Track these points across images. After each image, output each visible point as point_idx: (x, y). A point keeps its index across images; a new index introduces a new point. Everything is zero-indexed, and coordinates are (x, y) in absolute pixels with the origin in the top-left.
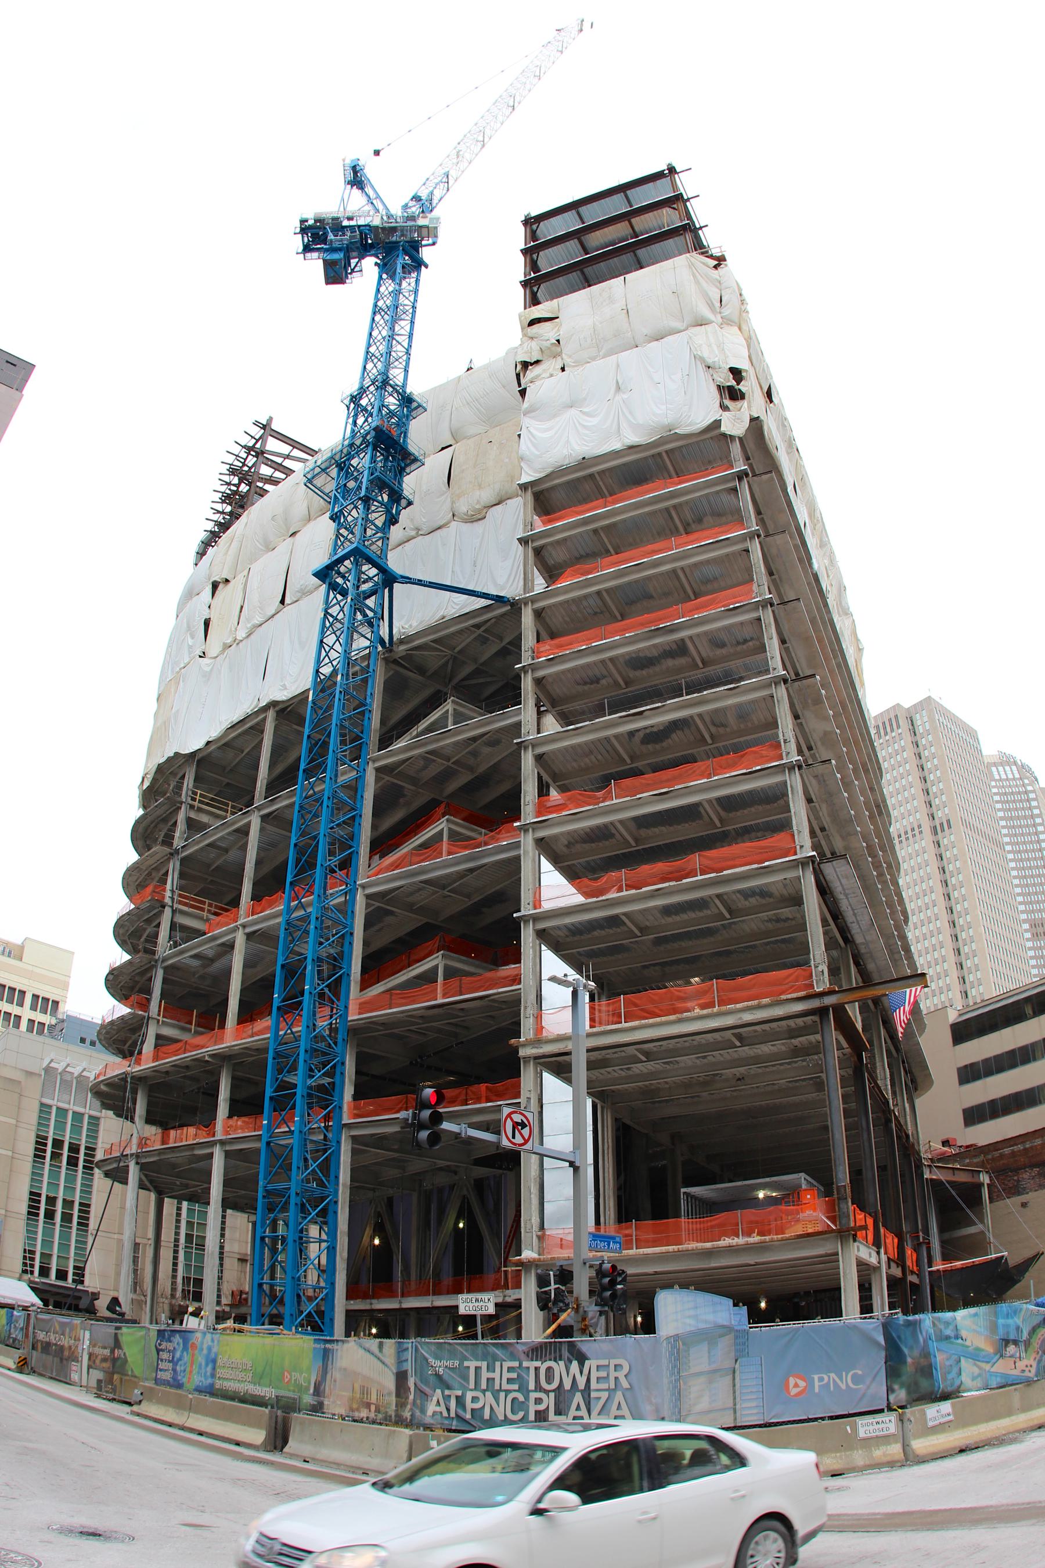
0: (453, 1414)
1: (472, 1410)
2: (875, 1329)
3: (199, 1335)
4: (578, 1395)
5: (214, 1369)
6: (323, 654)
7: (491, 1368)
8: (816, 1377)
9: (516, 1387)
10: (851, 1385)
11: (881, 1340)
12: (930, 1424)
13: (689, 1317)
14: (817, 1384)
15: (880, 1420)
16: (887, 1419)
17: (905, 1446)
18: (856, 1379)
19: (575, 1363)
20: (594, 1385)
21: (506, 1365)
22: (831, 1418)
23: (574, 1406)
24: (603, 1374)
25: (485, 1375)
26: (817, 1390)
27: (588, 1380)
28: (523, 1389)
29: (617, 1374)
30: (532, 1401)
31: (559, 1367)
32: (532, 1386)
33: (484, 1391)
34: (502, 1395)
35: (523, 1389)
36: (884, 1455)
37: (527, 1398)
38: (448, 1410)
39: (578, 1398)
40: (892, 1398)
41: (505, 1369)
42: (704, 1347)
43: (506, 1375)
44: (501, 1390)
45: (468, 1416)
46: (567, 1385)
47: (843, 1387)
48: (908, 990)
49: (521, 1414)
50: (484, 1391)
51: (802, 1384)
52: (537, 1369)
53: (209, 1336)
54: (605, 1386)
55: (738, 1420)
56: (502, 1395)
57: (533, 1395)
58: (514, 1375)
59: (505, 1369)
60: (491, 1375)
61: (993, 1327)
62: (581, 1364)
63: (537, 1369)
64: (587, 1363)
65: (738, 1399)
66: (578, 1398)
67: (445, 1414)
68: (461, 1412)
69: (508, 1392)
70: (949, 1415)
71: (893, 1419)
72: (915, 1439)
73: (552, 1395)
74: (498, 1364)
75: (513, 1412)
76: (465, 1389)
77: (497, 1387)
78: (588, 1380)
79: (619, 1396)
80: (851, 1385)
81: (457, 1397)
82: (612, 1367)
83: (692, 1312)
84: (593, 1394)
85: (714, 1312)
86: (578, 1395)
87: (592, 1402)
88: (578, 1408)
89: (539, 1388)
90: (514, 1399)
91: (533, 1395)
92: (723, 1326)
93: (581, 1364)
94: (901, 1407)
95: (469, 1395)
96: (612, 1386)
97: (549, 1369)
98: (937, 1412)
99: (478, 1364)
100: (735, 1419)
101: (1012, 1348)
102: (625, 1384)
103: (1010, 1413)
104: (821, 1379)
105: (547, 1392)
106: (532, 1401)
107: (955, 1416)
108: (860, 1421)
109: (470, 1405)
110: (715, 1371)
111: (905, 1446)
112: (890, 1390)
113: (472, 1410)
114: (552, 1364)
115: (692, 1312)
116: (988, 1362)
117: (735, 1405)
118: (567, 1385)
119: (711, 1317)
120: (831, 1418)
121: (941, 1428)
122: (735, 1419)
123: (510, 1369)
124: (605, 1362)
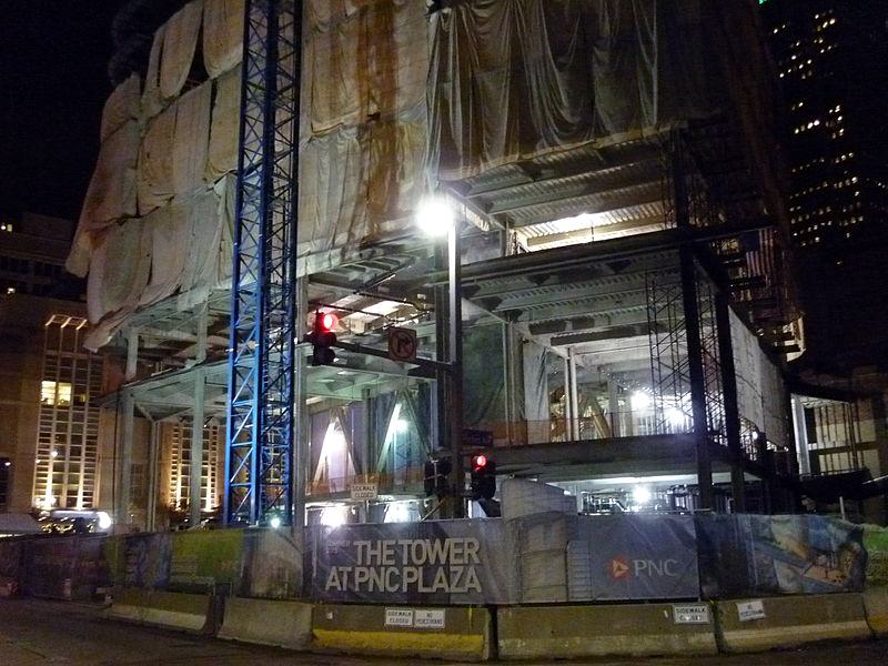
0: (345, 589)
1: (360, 583)
2: (688, 523)
3: (157, 537)
4: (441, 569)
5: (169, 566)
6: (251, 31)
7: (374, 547)
8: (636, 562)
9: (393, 562)
10: (667, 573)
11: (693, 533)
12: (742, 618)
13: (528, 502)
14: (637, 569)
15: (694, 608)
16: (701, 608)
17: (718, 637)
18: (672, 568)
19: (438, 541)
20: (452, 561)
21: (385, 543)
22: (651, 601)
23: (437, 581)
24: (460, 551)
25: (370, 552)
26: (637, 574)
27: (448, 557)
28: (399, 565)
29: (470, 551)
30: (405, 574)
31: (426, 544)
32: (405, 562)
33: (369, 567)
34: (383, 569)
35: (399, 565)
36: (699, 642)
37: (401, 572)
38: (341, 583)
39: (441, 573)
40: (704, 589)
41: (385, 547)
42: (540, 529)
43: (386, 552)
44: (381, 565)
45: (357, 589)
46: (432, 561)
47: (660, 572)
48: (760, 230)
49: (397, 586)
50: (369, 567)
51: (625, 568)
52: (409, 546)
53: (165, 537)
54: (461, 562)
55: (571, 595)
56: (383, 569)
57: (406, 570)
58: (392, 552)
59: (385, 547)
60: (374, 552)
61: (805, 536)
62: (443, 543)
63: (409, 546)
64: (447, 540)
65: (569, 578)
66: (441, 573)
67: (339, 589)
68: (351, 587)
69: (387, 567)
70: (760, 612)
71: (706, 608)
72: (729, 630)
73: (421, 569)
74: (379, 542)
75: (391, 585)
76: (354, 565)
77: (379, 563)
78: (448, 557)
79: (472, 569)
80: (667, 573)
81: (349, 573)
82: (466, 545)
83: (530, 499)
84: (452, 569)
85: (548, 499)
86: (441, 569)
87: (451, 575)
88: (441, 581)
89: (411, 564)
90: (392, 573)
91: (406, 570)
92: (558, 512)
93: (443, 543)
94: (714, 599)
95: (358, 570)
96: (467, 562)
97: (419, 546)
98: (751, 608)
99: (365, 543)
100: (568, 595)
101: (822, 559)
102: (476, 560)
103: (824, 620)
104: (641, 564)
105: (417, 567)
106: (405, 574)
107: (766, 613)
108: (676, 608)
109: (358, 580)
110: (551, 551)
111: (718, 637)
112: (703, 582)
113: (360, 583)
114: (420, 542)
115: (530, 499)
116: (802, 567)
117: (567, 582)
118: (432, 561)
119: (545, 503)
120: (651, 601)
121: (751, 624)
122: (568, 595)
123: (389, 547)
124: (460, 540)
